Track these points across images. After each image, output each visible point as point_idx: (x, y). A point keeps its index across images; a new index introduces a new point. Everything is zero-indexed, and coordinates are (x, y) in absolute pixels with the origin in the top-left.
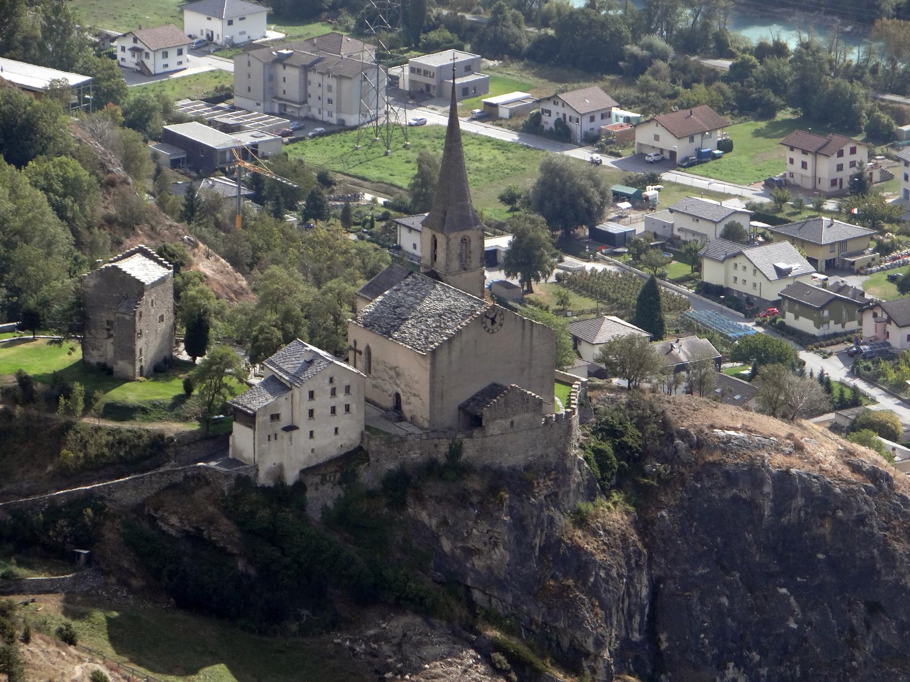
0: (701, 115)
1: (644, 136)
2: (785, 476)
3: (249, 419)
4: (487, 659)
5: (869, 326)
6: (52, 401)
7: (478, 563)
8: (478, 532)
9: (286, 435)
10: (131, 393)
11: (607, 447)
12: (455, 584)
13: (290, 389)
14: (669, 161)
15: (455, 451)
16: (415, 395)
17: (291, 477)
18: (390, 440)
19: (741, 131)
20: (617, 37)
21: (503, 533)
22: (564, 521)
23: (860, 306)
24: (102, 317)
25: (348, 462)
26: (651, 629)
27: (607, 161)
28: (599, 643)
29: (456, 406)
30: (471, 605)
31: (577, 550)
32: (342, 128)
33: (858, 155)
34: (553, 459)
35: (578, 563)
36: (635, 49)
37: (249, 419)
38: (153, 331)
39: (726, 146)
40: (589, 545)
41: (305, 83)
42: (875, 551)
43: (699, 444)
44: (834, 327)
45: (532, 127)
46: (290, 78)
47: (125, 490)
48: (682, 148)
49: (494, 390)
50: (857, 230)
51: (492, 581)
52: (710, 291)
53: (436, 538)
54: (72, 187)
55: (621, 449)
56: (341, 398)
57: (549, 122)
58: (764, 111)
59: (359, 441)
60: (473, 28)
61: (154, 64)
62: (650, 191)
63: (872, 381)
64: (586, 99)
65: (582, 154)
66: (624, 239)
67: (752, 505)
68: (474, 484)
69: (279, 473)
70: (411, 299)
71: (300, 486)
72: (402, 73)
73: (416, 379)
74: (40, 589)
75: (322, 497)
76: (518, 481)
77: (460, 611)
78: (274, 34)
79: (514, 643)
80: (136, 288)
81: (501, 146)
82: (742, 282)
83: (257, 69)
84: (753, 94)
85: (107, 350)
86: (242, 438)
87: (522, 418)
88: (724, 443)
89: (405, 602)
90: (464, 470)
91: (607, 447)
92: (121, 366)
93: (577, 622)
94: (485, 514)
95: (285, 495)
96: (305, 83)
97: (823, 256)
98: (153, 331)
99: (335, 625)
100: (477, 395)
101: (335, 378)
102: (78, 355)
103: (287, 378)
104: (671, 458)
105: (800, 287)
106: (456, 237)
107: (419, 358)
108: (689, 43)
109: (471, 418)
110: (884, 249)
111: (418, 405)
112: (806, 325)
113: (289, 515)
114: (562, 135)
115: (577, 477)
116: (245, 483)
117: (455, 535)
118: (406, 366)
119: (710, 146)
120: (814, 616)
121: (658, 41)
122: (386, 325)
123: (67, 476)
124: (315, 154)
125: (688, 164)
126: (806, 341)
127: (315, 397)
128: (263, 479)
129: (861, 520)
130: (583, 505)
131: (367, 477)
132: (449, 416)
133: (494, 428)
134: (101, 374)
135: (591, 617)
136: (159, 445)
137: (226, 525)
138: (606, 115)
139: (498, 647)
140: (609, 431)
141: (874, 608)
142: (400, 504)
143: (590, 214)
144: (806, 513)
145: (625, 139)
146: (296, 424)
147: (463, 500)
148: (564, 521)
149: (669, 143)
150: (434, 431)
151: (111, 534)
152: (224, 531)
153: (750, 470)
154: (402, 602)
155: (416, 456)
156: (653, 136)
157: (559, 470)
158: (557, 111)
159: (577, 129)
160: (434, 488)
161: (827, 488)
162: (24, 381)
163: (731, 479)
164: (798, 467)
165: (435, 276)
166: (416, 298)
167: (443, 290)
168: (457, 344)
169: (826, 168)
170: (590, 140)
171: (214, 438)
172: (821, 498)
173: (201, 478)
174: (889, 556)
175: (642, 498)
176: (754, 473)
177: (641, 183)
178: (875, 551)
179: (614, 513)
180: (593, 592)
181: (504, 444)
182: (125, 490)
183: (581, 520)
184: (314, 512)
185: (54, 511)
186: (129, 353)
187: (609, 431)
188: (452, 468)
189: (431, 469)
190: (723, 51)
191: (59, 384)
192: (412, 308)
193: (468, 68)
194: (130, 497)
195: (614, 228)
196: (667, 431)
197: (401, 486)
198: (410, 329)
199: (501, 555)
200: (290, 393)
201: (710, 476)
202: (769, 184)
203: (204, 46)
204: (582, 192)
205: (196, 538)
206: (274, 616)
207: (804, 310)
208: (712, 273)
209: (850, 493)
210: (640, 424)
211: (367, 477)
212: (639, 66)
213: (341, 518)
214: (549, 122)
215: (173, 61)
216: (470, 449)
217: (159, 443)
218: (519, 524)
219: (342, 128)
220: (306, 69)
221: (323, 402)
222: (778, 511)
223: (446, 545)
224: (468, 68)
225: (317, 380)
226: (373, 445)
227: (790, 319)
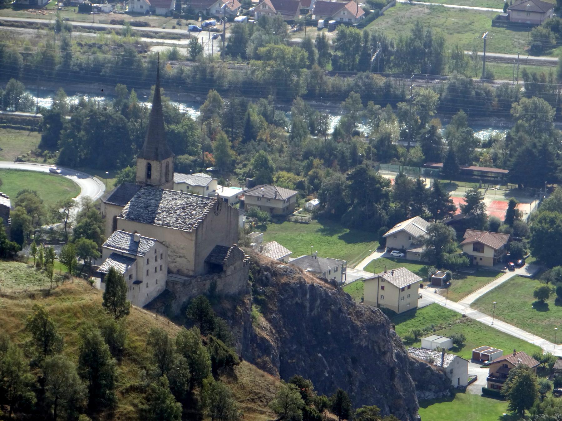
9: (136, 287)
13: (135, 260)
16: (180, 257)
29: (203, 261)
42: (349, 327)
59: (165, 287)
67: (301, 306)
70: (153, 201)
73: (182, 246)
88: (284, 271)
100: (211, 253)
101: (157, 250)
103: (128, 252)
107: (185, 235)
120: (334, 369)
127: (150, 263)
141: (354, 361)
144: (321, 308)
153: (301, 286)
166: (156, 200)
167: (173, 194)
168: (205, 223)
178: (349, 327)
192: (157, 206)
200: (135, 263)
201: (286, 291)
218: (267, 329)
222: (311, 310)
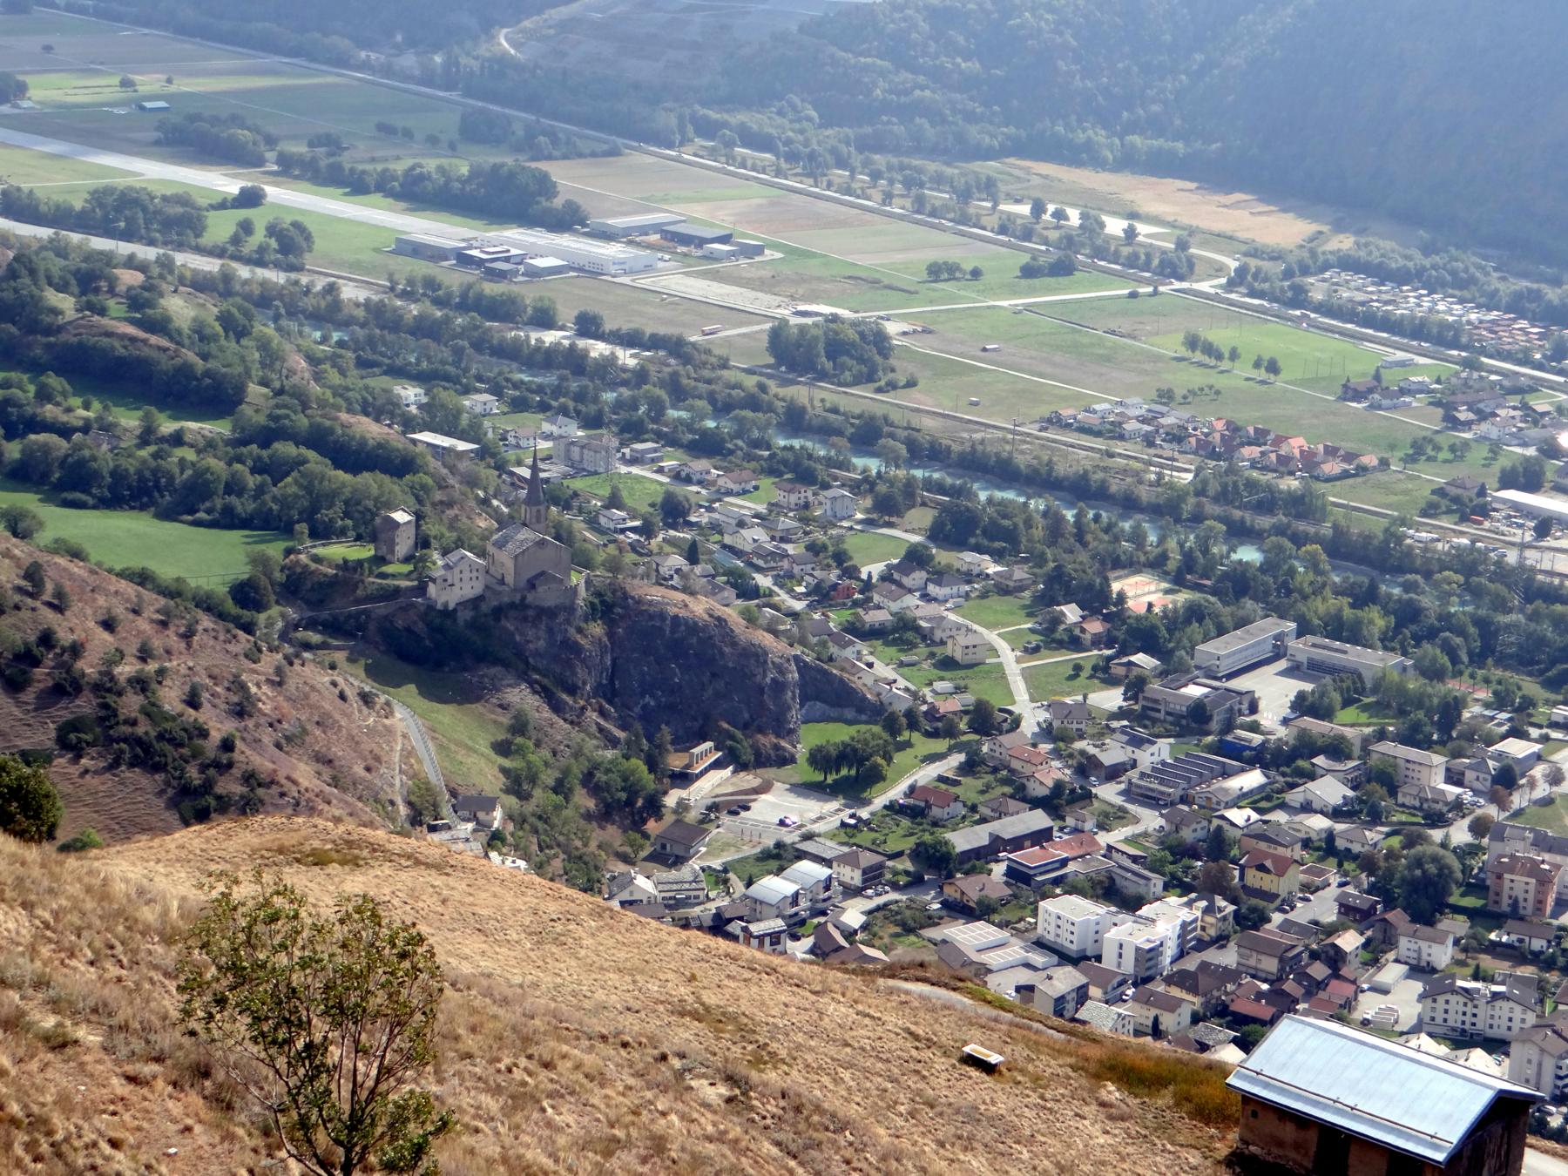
0: (746, 474)
1: (721, 482)
2: (676, 617)
3: (434, 581)
4: (531, 687)
5: (785, 564)
6: (355, 570)
7: (531, 646)
8: (531, 633)
10: (389, 569)
11: (596, 601)
12: (520, 654)
14: (730, 493)
15: (524, 598)
17: (451, 606)
18: (495, 593)
19: (766, 482)
20: (723, 441)
21: (542, 633)
22: (572, 631)
23: (785, 555)
24: (382, 536)
25: (476, 602)
26: (611, 679)
27: (704, 492)
28: (584, 683)
30: (527, 663)
31: (576, 643)
32: (596, 473)
33: (808, 493)
34: (567, 602)
35: (576, 649)
36: (729, 446)
37: (434, 581)
38: (404, 544)
39: (756, 488)
40: (583, 642)
41: (582, 454)
43: (639, 602)
44: (772, 564)
45: (677, 476)
46: (576, 451)
47: (381, 609)
48: (736, 488)
49: (543, 573)
50: (796, 524)
51: (537, 654)
52: (725, 546)
53: (513, 635)
54: (424, 487)
55: (603, 602)
56: (475, 574)
57: (683, 474)
58: (779, 474)
60: (666, 434)
61: (523, 443)
62: (717, 505)
63: (781, 587)
64: (700, 465)
65: (695, 488)
66: (696, 524)
67: (661, 629)
68: (531, 613)
69: (446, 605)
71: (455, 610)
72: (627, 451)
74: (338, 648)
75: (465, 615)
76: (551, 613)
77: (522, 666)
78: (580, 433)
79: (545, 681)
80: (396, 525)
81: (661, 484)
82: (739, 544)
83: (562, 447)
84: (774, 468)
85: (384, 550)
86: (432, 590)
87: (554, 586)
89: (498, 661)
90: (527, 607)
91: (596, 601)
92: (389, 557)
93: (574, 674)
94: (534, 625)
95: (447, 614)
96: (582, 454)
97: (778, 535)
98: (404, 544)
99: (465, 669)
102: (372, 552)
104: (626, 607)
105: (760, 547)
106: (534, 509)
108: (757, 444)
109: (532, 585)
110: (806, 533)
111: (510, 579)
112: (761, 563)
113: (449, 622)
114: (688, 480)
115: (579, 612)
116: (431, 608)
117: (522, 634)
118: (505, 560)
119: (749, 487)
121: (740, 443)
122: (500, 545)
123: (358, 602)
124: (578, 484)
125: (738, 494)
126: (759, 569)
128: (439, 607)
129: (711, 638)
130: (583, 625)
131: (484, 607)
132: (523, 583)
133: (540, 589)
134: (380, 560)
135: (581, 672)
136: (397, 591)
137: (421, 625)
138: (708, 472)
139: (537, 682)
140: (599, 594)
141: (714, 675)
142: (498, 620)
143: (685, 513)
145: (714, 483)
146: (456, 582)
147: (525, 619)
148: (572, 631)
149: (731, 485)
150: (515, 590)
151: (372, 627)
152: (420, 628)
154: (1051, 773)
155: (506, 599)
156: (726, 483)
157: (571, 609)
158: (687, 470)
159: (695, 478)
160: (512, 613)
161: (696, 623)
162: (346, 561)
163: (651, 617)
164: (683, 613)
165: (525, 525)
169: (793, 498)
170: (700, 483)
171: (421, 589)
172: (693, 627)
173: (413, 605)
174: (722, 653)
175: (611, 623)
176: (662, 616)
177: (714, 501)
179: (597, 629)
180: (583, 661)
181: (546, 596)
182: (381, 609)
183: (580, 631)
184: (461, 622)
185: (350, 616)
186: (392, 552)
187: (599, 594)
188: (520, 607)
189: (512, 605)
190: (768, 448)
191: (360, 563)
193: (655, 450)
194: (383, 612)
195: (693, 519)
196: (626, 596)
197: (498, 612)
198: (510, 546)
199: (542, 643)
202: (770, 504)
203: (548, 437)
204: (680, 503)
205: (408, 630)
206: (439, 665)
207: (760, 556)
208: (728, 540)
209: (706, 626)
210: (614, 592)
211: (484, 607)
212: (731, 452)
213: (472, 625)
214: (683, 474)
215: (531, 442)
216: (530, 598)
217: (397, 590)
218: (550, 631)
219: (596, 473)
220: (583, 447)
221: (466, 575)
222: (673, 632)
223: (518, 638)
224: (655, 450)
225: (464, 566)
226: (488, 594)
227: (755, 560)
